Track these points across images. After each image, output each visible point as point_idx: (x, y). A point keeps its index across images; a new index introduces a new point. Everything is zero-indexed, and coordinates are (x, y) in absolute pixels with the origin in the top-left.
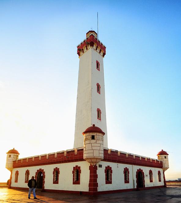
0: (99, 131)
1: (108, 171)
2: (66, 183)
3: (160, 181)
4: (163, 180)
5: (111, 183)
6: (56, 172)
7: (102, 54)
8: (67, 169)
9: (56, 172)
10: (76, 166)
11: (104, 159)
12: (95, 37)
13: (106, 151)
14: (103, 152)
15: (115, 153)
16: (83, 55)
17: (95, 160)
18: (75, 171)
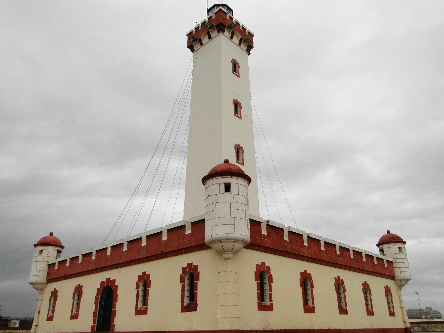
0: (240, 174)
5: (270, 308)
6: (144, 282)
7: (244, 47)
8: (166, 274)
9: (144, 282)
10: (188, 264)
12: (228, 16)
13: (255, 224)
15: (275, 230)
16: (202, 51)
18: (186, 278)
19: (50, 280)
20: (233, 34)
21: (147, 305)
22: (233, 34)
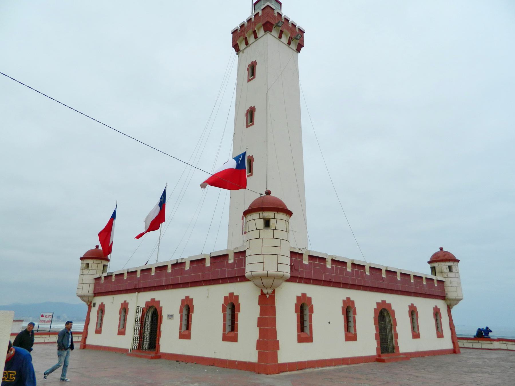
1: (303, 308)
2: (207, 339)
3: (440, 335)
4: (450, 334)
6: (187, 308)
7: (294, 46)
8: (208, 300)
9: (187, 308)
11: (291, 277)
12: (276, 12)
14: (288, 261)
17: (269, 281)
19: (96, 294)
20: (281, 32)
21: (190, 330)
22: (281, 32)
